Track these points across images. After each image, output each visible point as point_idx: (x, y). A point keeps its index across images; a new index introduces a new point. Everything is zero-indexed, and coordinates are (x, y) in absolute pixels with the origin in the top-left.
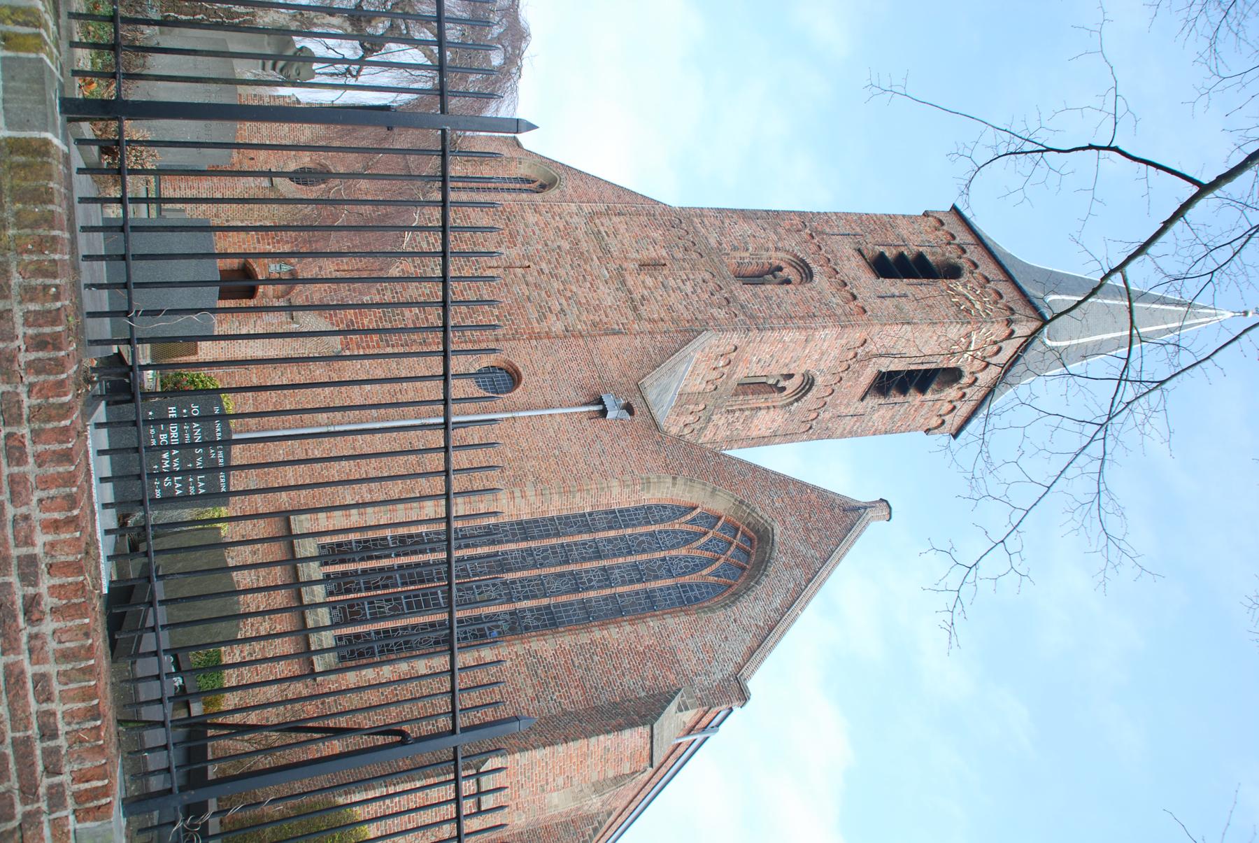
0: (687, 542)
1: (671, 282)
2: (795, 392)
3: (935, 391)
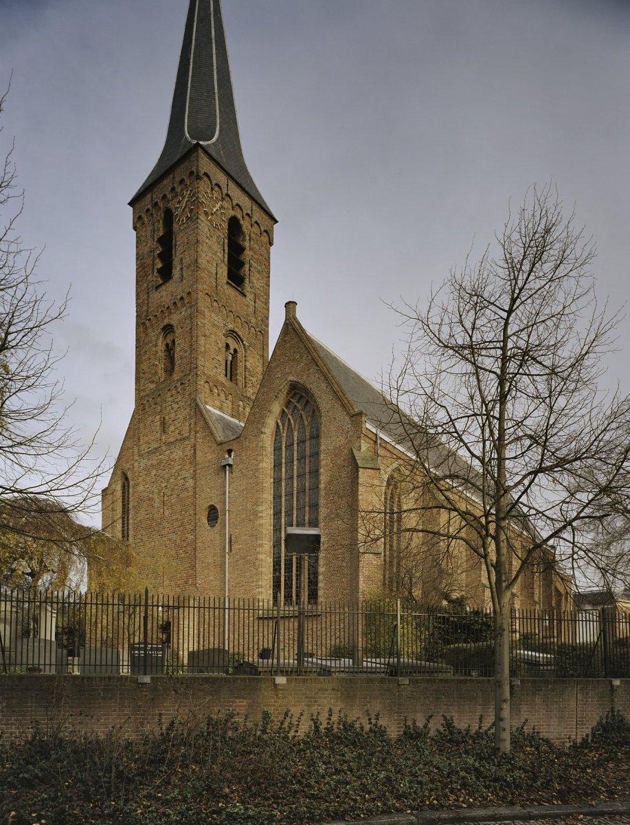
0: (292, 431)
1: (173, 416)
2: (238, 342)
3: (244, 240)
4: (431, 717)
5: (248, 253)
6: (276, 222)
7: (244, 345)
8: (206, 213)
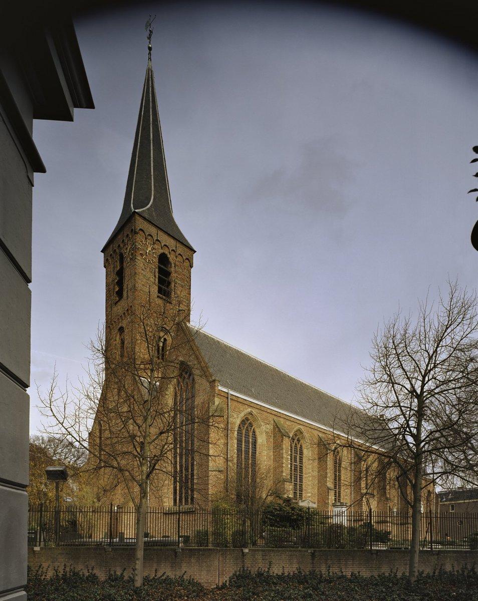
3: (171, 267)
4: (125, 569)
5: (174, 275)
6: (195, 252)
7: (171, 335)
8: (142, 255)
